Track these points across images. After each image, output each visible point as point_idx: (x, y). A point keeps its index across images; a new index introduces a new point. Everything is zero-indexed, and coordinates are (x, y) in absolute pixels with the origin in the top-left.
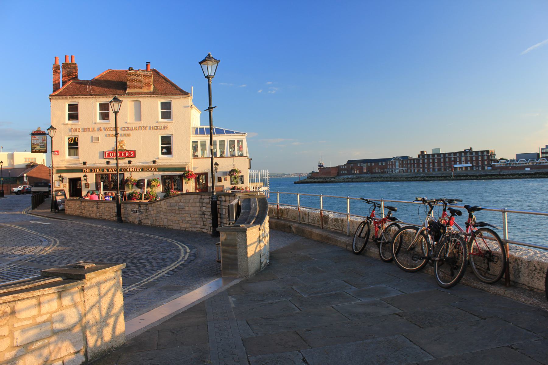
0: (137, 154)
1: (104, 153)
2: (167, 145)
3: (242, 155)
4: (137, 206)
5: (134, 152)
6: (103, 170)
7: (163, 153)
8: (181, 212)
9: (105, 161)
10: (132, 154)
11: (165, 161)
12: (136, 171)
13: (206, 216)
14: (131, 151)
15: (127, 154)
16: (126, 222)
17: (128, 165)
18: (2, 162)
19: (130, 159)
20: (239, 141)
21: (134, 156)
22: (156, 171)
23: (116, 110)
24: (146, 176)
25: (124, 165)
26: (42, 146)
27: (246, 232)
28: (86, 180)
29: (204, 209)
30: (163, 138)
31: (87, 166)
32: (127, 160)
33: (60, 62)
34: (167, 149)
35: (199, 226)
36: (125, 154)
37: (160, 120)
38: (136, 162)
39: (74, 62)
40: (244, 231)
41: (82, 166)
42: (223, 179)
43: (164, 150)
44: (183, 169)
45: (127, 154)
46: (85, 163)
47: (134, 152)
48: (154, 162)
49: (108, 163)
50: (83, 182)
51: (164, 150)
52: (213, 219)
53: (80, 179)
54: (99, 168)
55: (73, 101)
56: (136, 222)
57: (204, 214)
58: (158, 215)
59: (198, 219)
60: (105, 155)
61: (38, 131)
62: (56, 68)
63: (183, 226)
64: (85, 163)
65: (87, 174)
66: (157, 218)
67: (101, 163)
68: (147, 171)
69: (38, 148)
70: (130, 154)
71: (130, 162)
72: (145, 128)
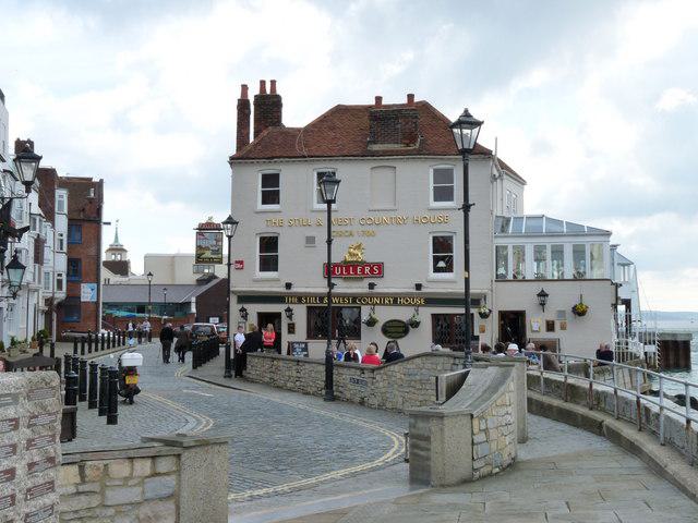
0: (386, 271)
5: (380, 266)
6: (321, 299)
10: (377, 269)
12: (384, 304)
15: (367, 270)
19: (372, 281)
21: (381, 274)
22: (420, 305)
24: (403, 314)
25: (360, 291)
28: (290, 317)
30: (293, 333)
31: (294, 290)
32: (366, 282)
36: (363, 271)
37: (261, 207)
38: (384, 286)
41: (283, 290)
42: (557, 326)
45: (367, 270)
46: (288, 286)
47: (380, 266)
48: (419, 287)
49: (372, 286)
61: (208, 224)
62: (243, 105)
64: (288, 286)
65: (291, 306)
67: (321, 287)
69: (208, 254)
70: (372, 271)
72: (399, 222)
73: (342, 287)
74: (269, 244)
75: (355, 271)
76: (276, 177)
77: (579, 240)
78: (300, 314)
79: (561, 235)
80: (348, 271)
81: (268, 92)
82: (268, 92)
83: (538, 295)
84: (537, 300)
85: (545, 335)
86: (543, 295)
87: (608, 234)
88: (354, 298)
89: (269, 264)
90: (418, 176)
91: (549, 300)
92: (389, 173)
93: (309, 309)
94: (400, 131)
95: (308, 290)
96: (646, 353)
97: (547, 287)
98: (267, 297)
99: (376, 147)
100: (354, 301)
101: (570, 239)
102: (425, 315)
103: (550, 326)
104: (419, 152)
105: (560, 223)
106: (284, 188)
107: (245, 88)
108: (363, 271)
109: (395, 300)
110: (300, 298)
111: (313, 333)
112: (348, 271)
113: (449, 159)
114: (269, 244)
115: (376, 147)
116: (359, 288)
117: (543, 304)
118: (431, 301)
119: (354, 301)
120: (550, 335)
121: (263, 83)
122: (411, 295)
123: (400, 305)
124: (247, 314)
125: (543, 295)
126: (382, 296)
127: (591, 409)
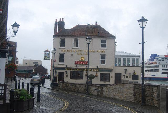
1: (75, 61)
3: (138, 66)
4: (97, 88)
8: (122, 92)
9: (75, 65)
13: (136, 95)
15: (85, 63)
16: (79, 92)
18: (26, 63)
23: (16, 31)
26: (48, 57)
29: (136, 91)
31: (68, 67)
33: (58, 21)
34: (103, 61)
35: (132, 100)
36: (84, 63)
41: (65, 67)
42: (129, 77)
44: (110, 70)
45: (85, 63)
46: (66, 66)
48: (97, 67)
49: (77, 66)
50: (65, 74)
52: (27, 86)
53: (64, 73)
54: (73, 68)
55: (63, 38)
56: (96, 94)
57: (136, 94)
58: (109, 92)
59: (132, 96)
60: (77, 63)
61: (47, 51)
62: (56, 23)
63: (122, 99)
64: (66, 66)
65: (67, 71)
66: (108, 94)
67: (74, 66)
69: (47, 58)
73: (79, 67)
74: (62, 56)
75: (82, 63)
78: (69, 72)
80: (81, 63)
81: (61, 21)
85: (126, 79)
88: (82, 69)
89: (62, 60)
93: (71, 72)
94: (95, 32)
95: (72, 67)
97: (127, 68)
102: (99, 73)
106: (66, 43)
107: (56, 19)
108: (84, 63)
109: (92, 70)
110: (69, 69)
112: (81, 63)
114: (62, 56)
118: (101, 70)
121: (60, 19)
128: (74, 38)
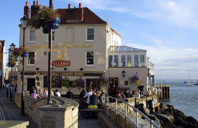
2: (90, 59)
7: (88, 63)
10: (68, 63)
11: (89, 68)
12: (70, 75)
14: (67, 61)
15: (64, 63)
17: (36, 71)
19: (65, 67)
20: (115, 56)
22: (82, 76)
25: (61, 71)
27: (64, 112)
33: (30, 6)
37: (87, 41)
38: (71, 69)
39: (39, 4)
40: (64, 110)
41: (36, 71)
42: (129, 83)
43: (89, 61)
44: (100, 74)
45: (64, 63)
46: (37, 69)
48: (81, 69)
51: (89, 61)
62: (26, 8)
68: (76, 76)
71: (65, 69)
76: (93, 30)
77: (136, 54)
79: (124, 52)
80: (57, 64)
82: (36, 5)
83: (122, 72)
84: (122, 74)
86: (124, 72)
87: (145, 51)
90: (82, 30)
91: (126, 74)
92: (72, 29)
96: (158, 92)
98: (93, 74)
99: (68, 21)
100: (60, 74)
101: (133, 53)
103: (126, 83)
104: (82, 23)
105: (131, 48)
111: (6, 84)
112: (57, 64)
113: (76, 25)
115: (68, 21)
116: (61, 69)
117: (124, 76)
119: (60, 74)
120: (127, 86)
121: (34, 2)
122: (79, 72)
123: (75, 76)
124: (38, 79)
125: (124, 72)
126: (69, 72)
127: (44, 106)
128: (87, 26)
